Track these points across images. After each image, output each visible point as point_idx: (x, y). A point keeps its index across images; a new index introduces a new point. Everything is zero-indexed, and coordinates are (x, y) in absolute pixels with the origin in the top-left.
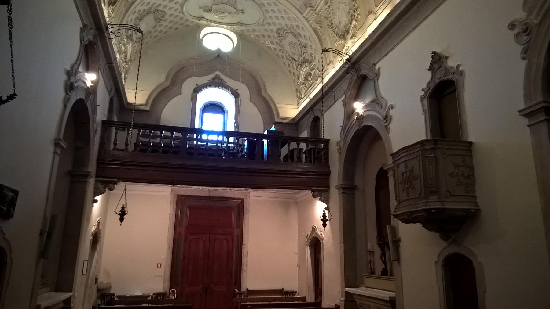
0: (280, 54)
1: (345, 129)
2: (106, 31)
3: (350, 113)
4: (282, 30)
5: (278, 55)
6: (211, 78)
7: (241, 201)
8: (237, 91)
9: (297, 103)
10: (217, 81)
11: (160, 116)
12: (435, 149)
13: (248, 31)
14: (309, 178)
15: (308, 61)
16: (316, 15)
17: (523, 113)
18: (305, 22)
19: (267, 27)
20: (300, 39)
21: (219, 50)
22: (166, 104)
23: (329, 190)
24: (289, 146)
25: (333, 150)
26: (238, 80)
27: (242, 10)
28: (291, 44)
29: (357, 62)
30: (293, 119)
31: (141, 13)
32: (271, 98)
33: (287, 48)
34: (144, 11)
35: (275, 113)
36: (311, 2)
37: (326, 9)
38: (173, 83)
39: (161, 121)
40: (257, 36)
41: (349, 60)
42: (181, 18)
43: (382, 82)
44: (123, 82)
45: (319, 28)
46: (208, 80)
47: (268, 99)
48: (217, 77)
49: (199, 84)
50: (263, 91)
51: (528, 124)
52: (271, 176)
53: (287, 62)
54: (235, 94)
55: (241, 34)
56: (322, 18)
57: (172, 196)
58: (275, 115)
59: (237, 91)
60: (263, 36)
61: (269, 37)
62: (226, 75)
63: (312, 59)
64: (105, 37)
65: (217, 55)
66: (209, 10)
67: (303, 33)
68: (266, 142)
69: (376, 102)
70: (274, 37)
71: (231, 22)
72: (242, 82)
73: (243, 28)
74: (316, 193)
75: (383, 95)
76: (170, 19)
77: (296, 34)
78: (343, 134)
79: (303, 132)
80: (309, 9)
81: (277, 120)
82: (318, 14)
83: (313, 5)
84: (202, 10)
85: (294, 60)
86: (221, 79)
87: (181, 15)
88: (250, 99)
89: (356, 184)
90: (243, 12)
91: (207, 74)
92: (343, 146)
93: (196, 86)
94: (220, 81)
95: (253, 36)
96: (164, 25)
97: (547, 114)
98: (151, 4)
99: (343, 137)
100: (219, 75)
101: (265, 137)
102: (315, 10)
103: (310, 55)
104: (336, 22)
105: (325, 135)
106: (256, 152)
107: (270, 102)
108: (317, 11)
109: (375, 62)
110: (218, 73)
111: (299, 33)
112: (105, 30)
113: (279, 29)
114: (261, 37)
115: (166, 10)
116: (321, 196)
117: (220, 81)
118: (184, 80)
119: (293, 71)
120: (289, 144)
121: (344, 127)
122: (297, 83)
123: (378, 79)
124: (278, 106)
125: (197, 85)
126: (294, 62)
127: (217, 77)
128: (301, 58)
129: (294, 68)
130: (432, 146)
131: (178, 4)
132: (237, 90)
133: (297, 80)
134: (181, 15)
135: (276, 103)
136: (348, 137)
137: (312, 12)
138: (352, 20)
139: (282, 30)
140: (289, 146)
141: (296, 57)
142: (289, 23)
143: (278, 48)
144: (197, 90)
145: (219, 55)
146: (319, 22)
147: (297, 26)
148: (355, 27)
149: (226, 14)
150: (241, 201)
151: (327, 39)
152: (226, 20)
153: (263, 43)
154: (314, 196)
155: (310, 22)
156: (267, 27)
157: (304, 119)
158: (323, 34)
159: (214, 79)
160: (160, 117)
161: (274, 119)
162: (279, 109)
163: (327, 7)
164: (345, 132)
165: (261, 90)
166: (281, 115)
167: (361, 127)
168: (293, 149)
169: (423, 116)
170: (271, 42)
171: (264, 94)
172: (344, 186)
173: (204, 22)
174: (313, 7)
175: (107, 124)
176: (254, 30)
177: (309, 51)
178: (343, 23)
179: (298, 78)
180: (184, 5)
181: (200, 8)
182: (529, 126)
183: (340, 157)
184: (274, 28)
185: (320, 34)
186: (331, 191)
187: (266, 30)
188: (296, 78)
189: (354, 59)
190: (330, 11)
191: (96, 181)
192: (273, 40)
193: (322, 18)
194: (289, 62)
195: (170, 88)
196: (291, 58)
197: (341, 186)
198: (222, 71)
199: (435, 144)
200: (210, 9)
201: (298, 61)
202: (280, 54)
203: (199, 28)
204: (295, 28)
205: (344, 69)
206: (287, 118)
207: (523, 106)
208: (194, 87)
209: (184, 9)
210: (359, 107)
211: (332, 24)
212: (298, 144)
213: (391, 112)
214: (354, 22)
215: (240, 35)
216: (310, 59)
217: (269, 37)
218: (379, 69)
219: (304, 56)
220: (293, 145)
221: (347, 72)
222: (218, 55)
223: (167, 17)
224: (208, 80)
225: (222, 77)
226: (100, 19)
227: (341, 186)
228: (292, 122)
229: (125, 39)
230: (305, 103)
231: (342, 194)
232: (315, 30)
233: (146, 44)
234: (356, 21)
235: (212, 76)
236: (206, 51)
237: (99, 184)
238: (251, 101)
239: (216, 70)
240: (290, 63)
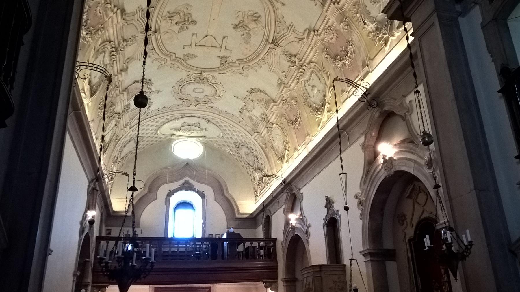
0: (238, 159)
1: (286, 233)
2: (103, 177)
3: (287, 222)
4: (238, 143)
5: (237, 160)
6: (181, 183)
7: (209, 289)
8: (204, 193)
9: (255, 200)
10: (186, 185)
11: (140, 219)
12: (320, 271)
13: (211, 141)
14: (264, 272)
15: (260, 168)
16: (261, 138)
17: (363, 253)
18: (255, 142)
19: (226, 140)
20: (253, 152)
21: (188, 160)
22: (144, 209)
23: (277, 281)
24: (244, 246)
25: (279, 247)
26: (204, 183)
27: (205, 129)
28: (246, 154)
29: (289, 183)
30: (252, 214)
31: (124, 143)
32: (232, 198)
33: (244, 156)
34: (127, 141)
35: (236, 210)
36: (258, 129)
37: (268, 136)
38: (150, 190)
39: (140, 224)
40: (219, 145)
41: (284, 182)
42: (156, 138)
43: (305, 203)
44: (109, 193)
45: (265, 148)
46: (180, 186)
47: (230, 198)
48: (187, 182)
49: (172, 189)
50: (225, 192)
51: (364, 261)
52: (229, 273)
53: (245, 166)
54: (202, 195)
55: (205, 143)
56: (267, 141)
57: (151, 289)
58: (236, 212)
59: (204, 193)
60: (224, 145)
61: (229, 146)
62: (193, 179)
63: (263, 168)
64: (102, 182)
65: (186, 163)
66: (179, 130)
67: (254, 148)
68: (225, 243)
69: (302, 219)
70: (233, 147)
71: (196, 136)
72: (208, 184)
73: (207, 139)
74: (267, 284)
75: (305, 215)
76: (147, 140)
77: (249, 147)
78: (285, 236)
79: (259, 226)
80: (256, 134)
81: (237, 216)
82: (263, 137)
83: (259, 131)
84: (173, 130)
85: (250, 165)
86: (190, 184)
87: (157, 136)
88: (215, 199)
89: (296, 277)
90: (206, 130)
91: (178, 180)
92: (285, 247)
93: (169, 191)
94: (189, 186)
95: (215, 145)
96: (142, 144)
97: (371, 257)
98: (132, 135)
99: (284, 239)
100: (188, 180)
101: (225, 240)
102: (261, 135)
103: (261, 164)
104: (276, 146)
105: (273, 236)
106: (217, 253)
107: (231, 200)
108: (262, 135)
109: (300, 188)
110: (187, 178)
111: (251, 147)
112: (102, 176)
113: (235, 142)
114: (223, 146)
115: (144, 135)
116: (271, 286)
117: (189, 186)
118: (159, 187)
119: (249, 172)
120: (244, 244)
121: (285, 231)
122: (254, 183)
123: (302, 201)
124: (238, 203)
125: (169, 190)
126: (250, 166)
127: (187, 182)
128: (254, 165)
129: (250, 171)
130: (318, 269)
131: (154, 130)
132: (203, 191)
133: (253, 180)
134: (157, 136)
135: (236, 200)
136: (287, 241)
137: (258, 136)
138: (286, 149)
139: (238, 143)
140: (244, 246)
141: (251, 163)
142: (243, 140)
143: (237, 155)
144: (170, 194)
145: (188, 165)
146: (265, 144)
147: (249, 142)
148: (287, 155)
149: (193, 131)
150: (209, 289)
151: (271, 157)
152: (192, 135)
153: (225, 150)
154: (266, 287)
155: (258, 142)
156: (226, 140)
157: (260, 216)
158: (268, 152)
159: (184, 184)
160: (140, 221)
161: (235, 216)
162: (239, 206)
163: (268, 135)
164: (286, 235)
165: (223, 190)
166: (241, 211)
167: (294, 235)
168: (248, 247)
169: (324, 238)
170: (230, 150)
171: (226, 195)
172: (286, 280)
173: (175, 137)
174: (259, 133)
175: (99, 239)
176: (217, 141)
177: (260, 162)
178: (280, 149)
179: (254, 179)
180: (158, 130)
181: (171, 129)
182: (364, 262)
183: (283, 254)
184: (232, 141)
185: (267, 152)
186: (279, 282)
187: (226, 142)
188: (252, 178)
189: (287, 181)
190: (271, 138)
191: (92, 286)
192: (232, 149)
193: (267, 141)
194: (247, 166)
195: (148, 194)
196: (248, 163)
197: (284, 279)
198: (190, 177)
199: (320, 268)
200: (180, 129)
201: (252, 167)
202: (238, 159)
203: (171, 142)
204: (248, 143)
205: (280, 189)
206: (246, 214)
207: (362, 250)
208: (168, 192)
209: (158, 132)
210: (293, 218)
211: (273, 147)
212: (252, 244)
213: (310, 230)
214: (287, 151)
215: (206, 145)
216: (261, 167)
217: (229, 146)
218: (302, 194)
219: (256, 164)
220: (248, 244)
221: (282, 191)
222: (187, 163)
223: (144, 139)
224: (180, 186)
225: (191, 181)
226: (92, 149)
227: (284, 279)
228: (251, 217)
229: (112, 165)
230: (260, 201)
231: (285, 286)
232: (262, 148)
233: (128, 159)
234: (288, 151)
235: (182, 181)
236: (177, 159)
237: (95, 288)
238: (215, 200)
239: (185, 176)
240: (247, 167)
